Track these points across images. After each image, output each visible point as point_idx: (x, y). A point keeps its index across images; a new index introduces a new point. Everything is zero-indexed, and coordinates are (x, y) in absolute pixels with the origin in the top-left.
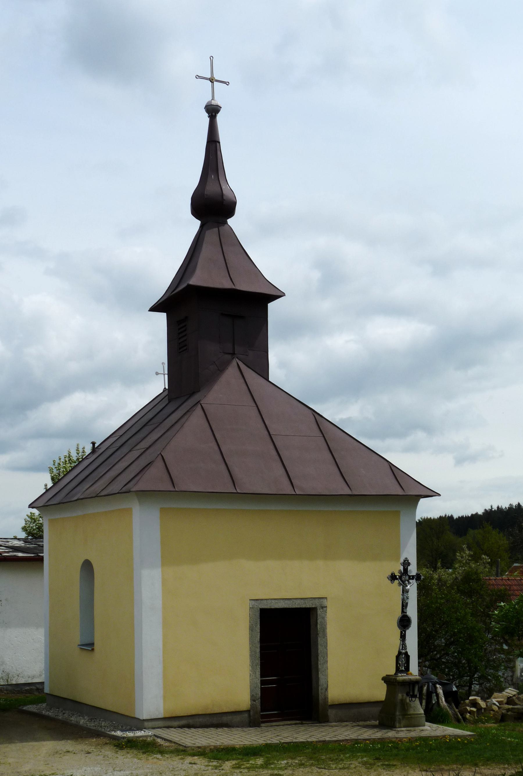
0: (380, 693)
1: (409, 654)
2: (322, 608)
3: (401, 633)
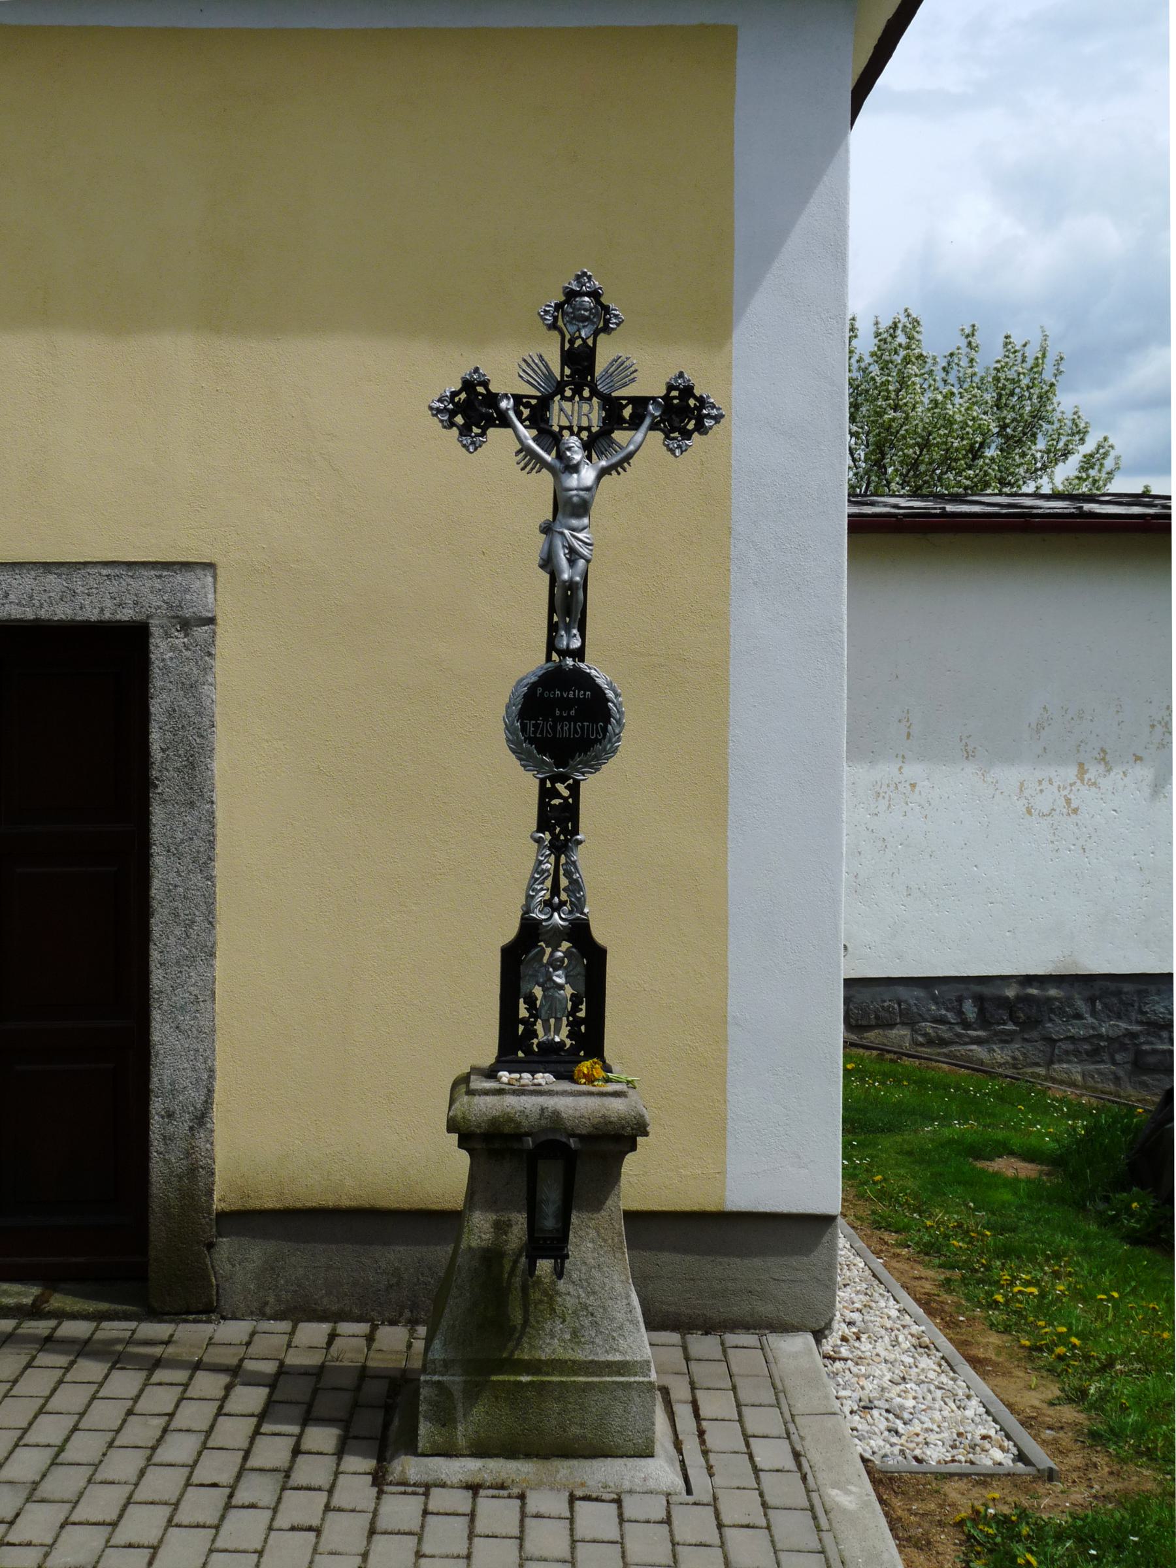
0: (440, 1172)
1: (599, 934)
2: (186, 625)
3: (546, 794)
